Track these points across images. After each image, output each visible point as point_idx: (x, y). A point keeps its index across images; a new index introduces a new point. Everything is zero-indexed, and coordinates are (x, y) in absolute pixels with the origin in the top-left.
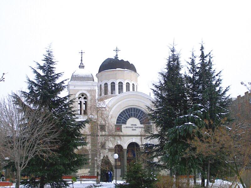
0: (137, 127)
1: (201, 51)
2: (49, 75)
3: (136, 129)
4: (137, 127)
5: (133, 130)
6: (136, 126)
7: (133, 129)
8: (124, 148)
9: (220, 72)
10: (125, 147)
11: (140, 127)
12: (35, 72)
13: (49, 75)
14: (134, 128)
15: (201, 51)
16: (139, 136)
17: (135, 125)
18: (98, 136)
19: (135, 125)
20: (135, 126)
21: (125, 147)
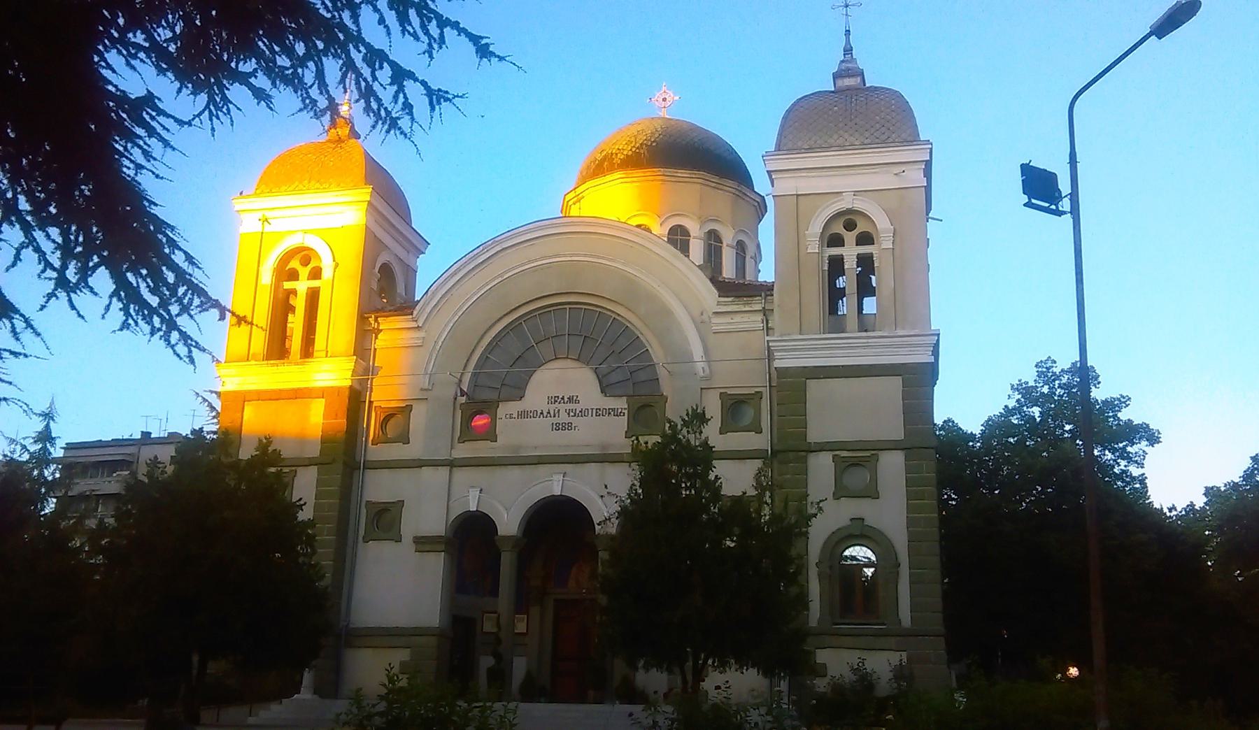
0: (583, 413)
1: (382, 26)
2: (641, 497)
3: (575, 421)
4: (583, 413)
5: (557, 427)
6: (578, 407)
7: (555, 420)
8: (502, 531)
9: (83, 317)
10: (509, 523)
11: (599, 412)
12: (59, 415)
13: (641, 497)
14: (564, 417)
15: (382, 26)
16: (628, 462)
17: (571, 399)
18: (336, 129)
19: (571, 399)
20: (571, 406)
21: (509, 523)
